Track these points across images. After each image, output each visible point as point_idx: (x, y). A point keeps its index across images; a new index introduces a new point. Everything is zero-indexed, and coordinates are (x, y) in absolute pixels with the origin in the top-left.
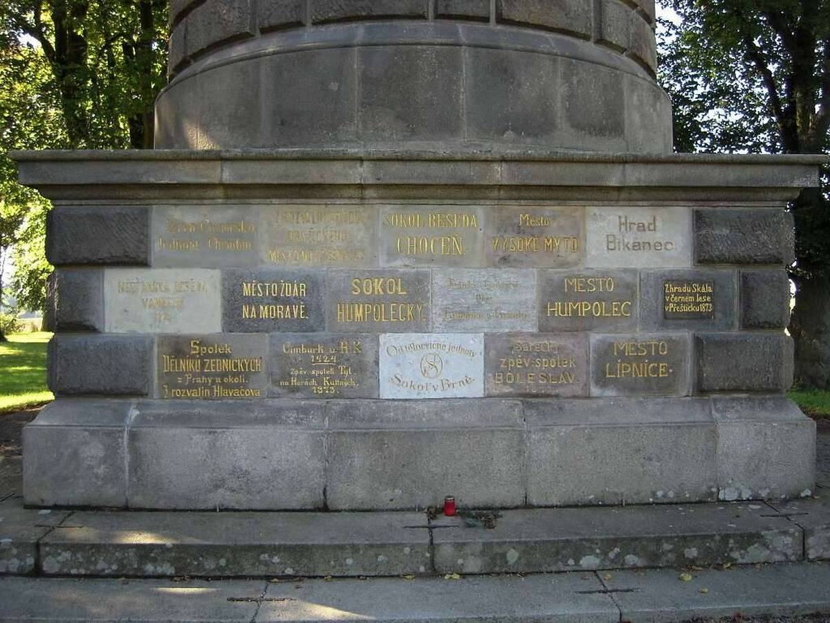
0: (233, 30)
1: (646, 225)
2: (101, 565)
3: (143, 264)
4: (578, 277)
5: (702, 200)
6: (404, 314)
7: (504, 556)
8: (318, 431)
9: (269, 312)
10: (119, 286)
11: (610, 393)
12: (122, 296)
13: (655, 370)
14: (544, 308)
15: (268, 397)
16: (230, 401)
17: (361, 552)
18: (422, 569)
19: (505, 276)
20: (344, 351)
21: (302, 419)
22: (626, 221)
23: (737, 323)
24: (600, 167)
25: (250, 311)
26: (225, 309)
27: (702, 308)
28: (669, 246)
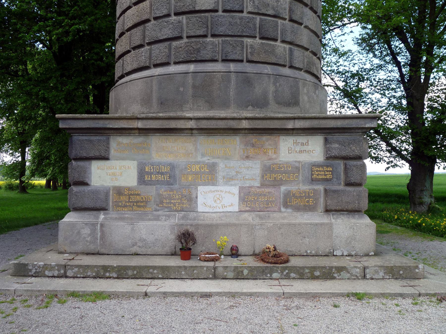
0: (142, 65)
1: (304, 143)
2: (89, 274)
3: (106, 158)
4: (276, 164)
5: (328, 133)
7: (242, 272)
8: (209, 67)
10: (97, 167)
11: (289, 210)
13: (308, 202)
14: (263, 177)
17: (188, 269)
18: (211, 276)
19: (247, 164)
21: (167, 219)
23: (342, 183)
25: (148, 177)
26: (138, 176)
27: (328, 177)
28: (314, 152)
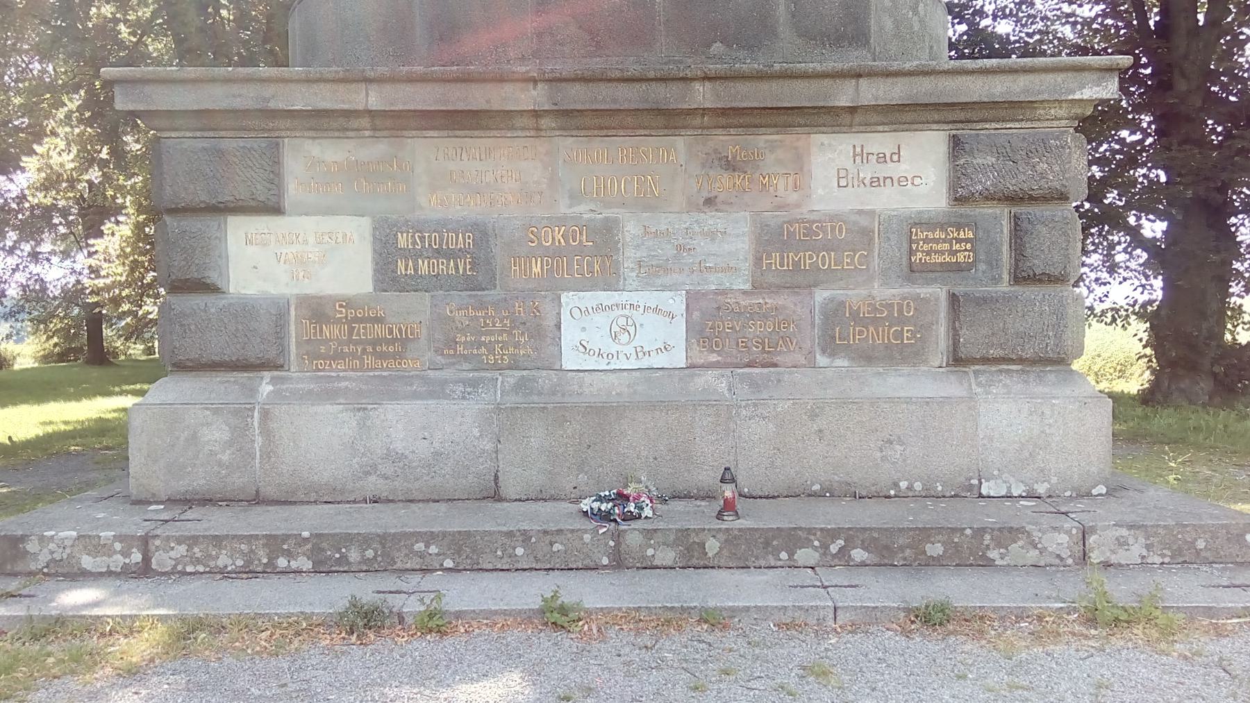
3: (275, 209)
5: (962, 122)
6: (590, 269)
7: (702, 545)
9: (429, 267)
10: (247, 236)
11: (841, 362)
12: (251, 250)
13: (899, 335)
15: (429, 369)
16: (385, 374)
20: (520, 314)
22: (862, 151)
23: (1006, 277)
24: (827, 82)
25: (407, 266)
26: (377, 264)
27: (961, 258)
28: (917, 181)
